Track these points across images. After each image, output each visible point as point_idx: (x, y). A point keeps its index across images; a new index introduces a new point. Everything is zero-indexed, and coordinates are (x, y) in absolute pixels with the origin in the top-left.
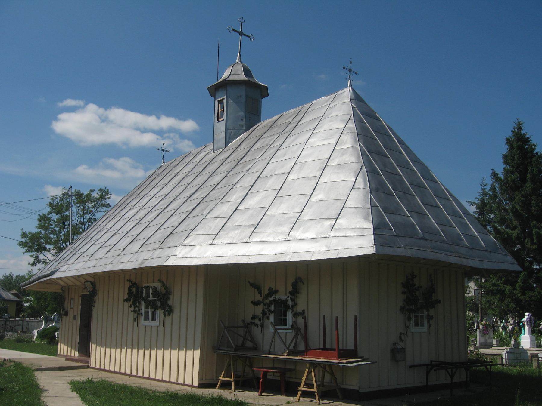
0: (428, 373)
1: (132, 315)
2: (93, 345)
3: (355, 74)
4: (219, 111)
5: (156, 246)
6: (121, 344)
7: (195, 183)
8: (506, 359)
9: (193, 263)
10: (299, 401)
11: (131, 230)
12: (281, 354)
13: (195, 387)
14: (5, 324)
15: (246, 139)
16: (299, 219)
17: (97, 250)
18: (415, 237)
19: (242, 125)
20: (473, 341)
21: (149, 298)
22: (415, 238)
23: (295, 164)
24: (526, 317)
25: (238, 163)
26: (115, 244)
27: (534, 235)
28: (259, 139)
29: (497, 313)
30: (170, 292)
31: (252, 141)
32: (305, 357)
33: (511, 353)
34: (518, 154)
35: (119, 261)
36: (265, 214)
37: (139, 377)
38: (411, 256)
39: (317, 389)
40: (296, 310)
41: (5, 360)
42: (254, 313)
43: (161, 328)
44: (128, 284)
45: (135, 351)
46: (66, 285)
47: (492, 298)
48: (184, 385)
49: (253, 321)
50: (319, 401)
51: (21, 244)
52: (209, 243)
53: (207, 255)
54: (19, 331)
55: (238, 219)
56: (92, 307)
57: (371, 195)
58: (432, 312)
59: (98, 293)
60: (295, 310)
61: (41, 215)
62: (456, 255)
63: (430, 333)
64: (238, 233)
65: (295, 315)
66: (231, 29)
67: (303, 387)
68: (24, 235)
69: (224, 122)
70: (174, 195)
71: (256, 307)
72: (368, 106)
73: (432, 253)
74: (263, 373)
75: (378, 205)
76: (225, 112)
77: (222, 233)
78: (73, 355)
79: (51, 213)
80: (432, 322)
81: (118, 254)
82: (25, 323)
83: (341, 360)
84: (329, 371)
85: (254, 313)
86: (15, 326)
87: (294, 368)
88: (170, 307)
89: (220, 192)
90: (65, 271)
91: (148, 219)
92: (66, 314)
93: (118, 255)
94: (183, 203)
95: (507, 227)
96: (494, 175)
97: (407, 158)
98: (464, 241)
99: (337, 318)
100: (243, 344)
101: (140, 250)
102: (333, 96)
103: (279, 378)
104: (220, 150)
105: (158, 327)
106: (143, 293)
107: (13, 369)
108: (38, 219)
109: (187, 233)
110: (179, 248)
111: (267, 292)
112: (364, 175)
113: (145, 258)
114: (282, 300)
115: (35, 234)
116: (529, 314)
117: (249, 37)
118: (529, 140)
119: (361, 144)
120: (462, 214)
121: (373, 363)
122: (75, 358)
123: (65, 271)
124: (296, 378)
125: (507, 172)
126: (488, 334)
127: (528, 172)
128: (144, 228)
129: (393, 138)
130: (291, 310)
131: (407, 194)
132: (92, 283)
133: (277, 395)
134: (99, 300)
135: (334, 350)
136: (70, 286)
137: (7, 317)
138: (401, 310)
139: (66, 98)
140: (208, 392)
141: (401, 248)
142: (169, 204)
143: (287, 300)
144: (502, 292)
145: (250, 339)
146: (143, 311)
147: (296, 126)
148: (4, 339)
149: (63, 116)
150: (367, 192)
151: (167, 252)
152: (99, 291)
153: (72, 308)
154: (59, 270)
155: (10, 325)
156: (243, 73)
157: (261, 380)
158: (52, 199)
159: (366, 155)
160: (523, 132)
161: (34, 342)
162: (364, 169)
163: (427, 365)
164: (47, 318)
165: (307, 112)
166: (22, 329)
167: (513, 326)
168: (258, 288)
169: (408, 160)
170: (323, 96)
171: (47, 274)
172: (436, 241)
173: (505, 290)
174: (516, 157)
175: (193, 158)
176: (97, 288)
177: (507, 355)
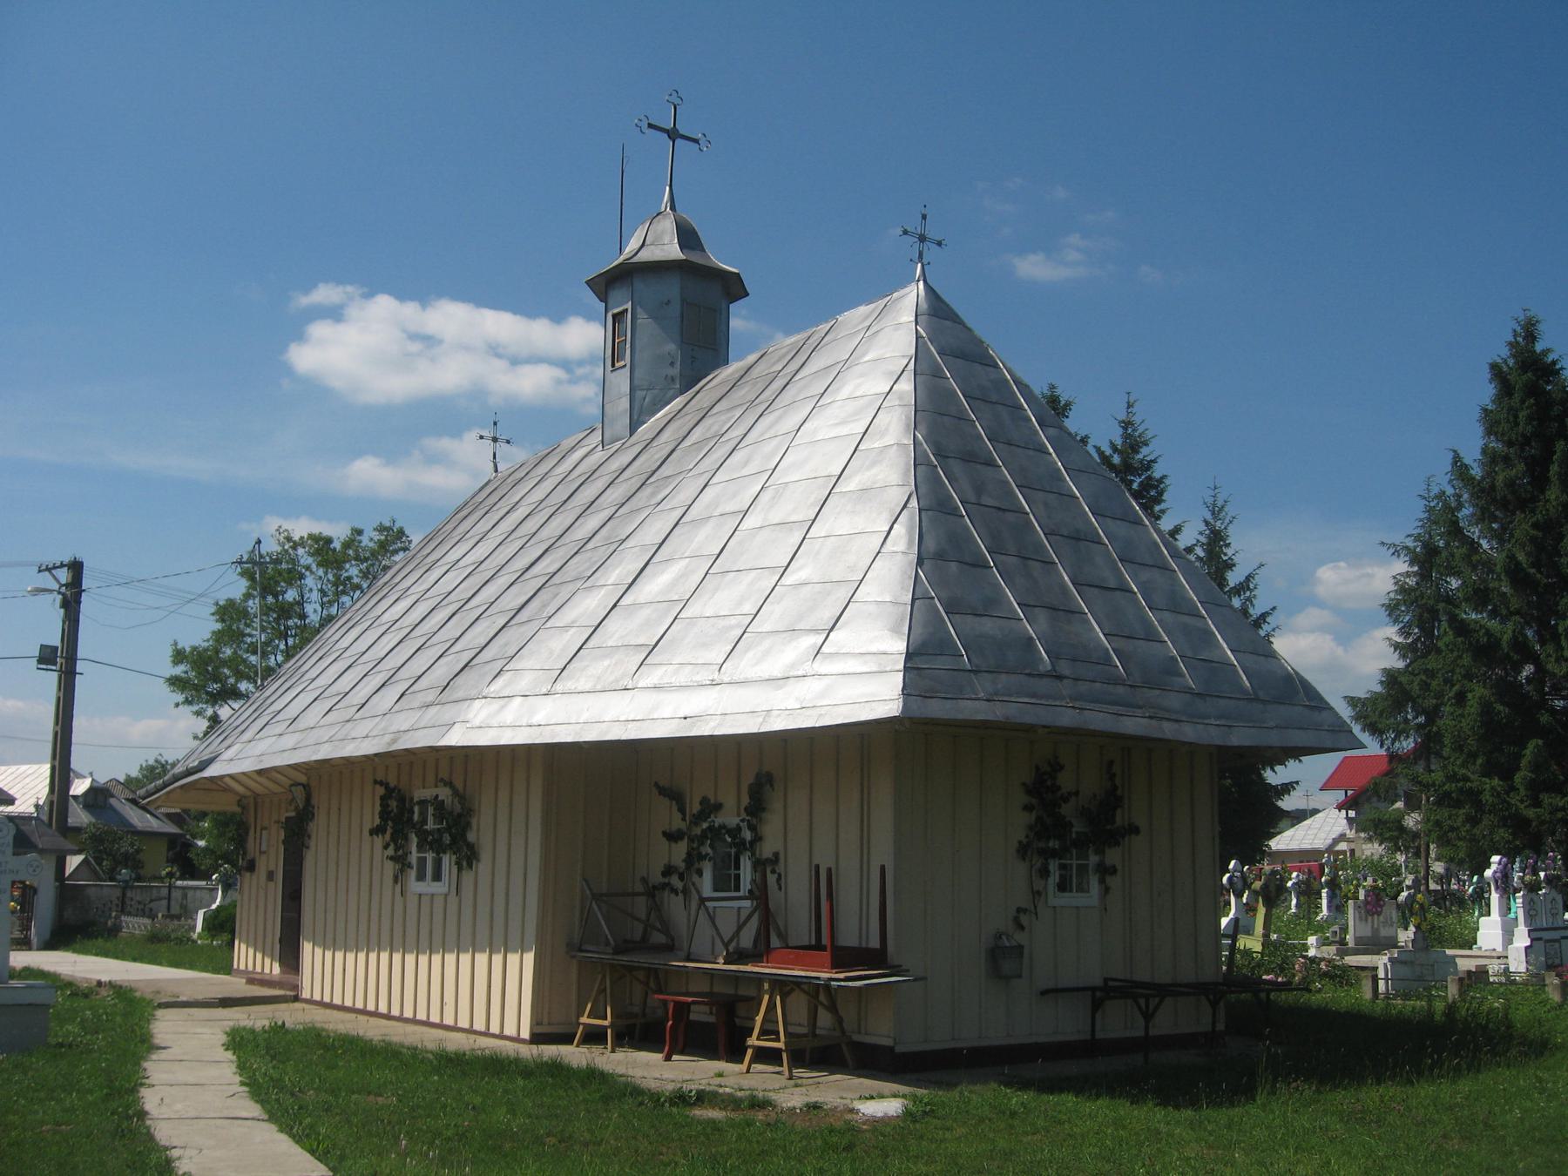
0: (1096, 1006)
1: (390, 867)
4: (617, 341)
5: (431, 696)
6: (366, 941)
7: (544, 533)
8: (1386, 979)
9: (503, 742)
10: (748, 1071)
11: (387, 655)
12: (713, 960)
13: (523, 1041)
14: (124, 895)
15: (678, 416)
16: (748, 630)
17: (308, 706)
18: (1027, 671)
19: (673, 379)
20: (1336, 932)
21: (427, 825)
22: (1026, 674)
23: (762, 488)
24: (1494, 867)
25: (646, 481)
26: (347, 691)
27: (1563, 637)
28: (703, 417)
29: (1462, 855)
30: (471, 810)
31: (690, 421)
32: (762, 967)
33: (1404, 963)
34: (1527, 408)
35: (346, 735)
36: (676, 618)
37: (407, 1021)
38: (1001, 719)
39: (786, 1043)
40: (761, 854)
41: (99, 983)
42: (670, 861)
43: (453, 898)
44: (381, 791)
45: (397, 957)
46: (249, 793)
47: (1446, 814)
48: (501, 1037)
49: (666, 880)
50: (790, 1071)
51: (175, 682)
52: (544, 690)
53: (535, 721)
54: (160, 915)
55: (615, 630)
56: (304, 849)
58: (1113, 856)
59: (316, 815)
60: (757, 853)
62: (1147, 715)
63: (1106, 909)
64: (609, 666)
65: (759, 865)
66: (647, 125)
67: (758, 1039)
68: (179, 656)
69: (627, 370)
70: (494, 564)
71: (673, 845)
73: (1070, 711)
74: (674, 1006)
75: (934, 595)
76: (628, 345)
77: (574, 665)
78: (267, 970)
80: (1114, 882)
81: (347, 718)
82: (176, 894)
83: (836, 973)
84: (825, 1003)
85: (670, 861)
86: (151, 901)
87: (755, 995)
88: (471, 847)
89: (591, 558)
90: (231, 760)
91: (429, 626)
92: (251, 867)
93: (348, 721)
94: (508, 588)
95: (1494, 614)
96: (1460, 469)
97: (1057, 464)
98: (1184, 676)
99: (883, 868)
100: (644, 938)
101: (397, 708)
102: (882, 303)
103: (712, 1019)
104: (618, 444)
105: (446, 895)
106: (413, 812)
107: (111, 1003)
109: (498, 665)
110: (477, 704)
111: (696, 808)
112: (911, 519)
113: (402, 729)
114: (729, 827)
115: (206, 650)
116: (1501, 859)
117: (696, 141)
118: (1557, 367)
119: (920, 437)
120: (1199, 605)
121: (915, 980)
122: (273, 979)
123: (231, 760)
125: (1492, 459)
126: (1379, 914)
127: (1555, 457)
128: (415, 649)
129: (1026, 410)
130: (749, 853)
132: (304, 786)
133: (711, 1059)
134: (318, 828)
136: (258, 795)
137: (128, 878)
138: (1018, 851)
141: (977, 702)
142: (480, 589)
143: (739, 829)
144: (1474, 796)
145: (658, 925)
146: (414, 857)
147: (788, 384)
148: (120, 934)
150: (911, 563)
151: (447, 713)
152: (318, 808)
153: (264, 852)
154: (218, 759)
155: (138, 898)
156: (676, 240)
157: (670, 1023)
159: (930, 464)
160: (1539, 347)
161: (194, 942)
162: (914, 503)
163: (1093, 989)
164: (227, 880)
165: (819, 347)
166: (169, 908)
167: (1413, 891)
168: (676, 797)
169: (1060, 469)
170: (861, 305)
171: (192, 768)
172: (1089, 681)
173: (1481, 792)
174: (1522, 414)
175: (559, 461)
176: (314, 801)
177: (1389, 967)
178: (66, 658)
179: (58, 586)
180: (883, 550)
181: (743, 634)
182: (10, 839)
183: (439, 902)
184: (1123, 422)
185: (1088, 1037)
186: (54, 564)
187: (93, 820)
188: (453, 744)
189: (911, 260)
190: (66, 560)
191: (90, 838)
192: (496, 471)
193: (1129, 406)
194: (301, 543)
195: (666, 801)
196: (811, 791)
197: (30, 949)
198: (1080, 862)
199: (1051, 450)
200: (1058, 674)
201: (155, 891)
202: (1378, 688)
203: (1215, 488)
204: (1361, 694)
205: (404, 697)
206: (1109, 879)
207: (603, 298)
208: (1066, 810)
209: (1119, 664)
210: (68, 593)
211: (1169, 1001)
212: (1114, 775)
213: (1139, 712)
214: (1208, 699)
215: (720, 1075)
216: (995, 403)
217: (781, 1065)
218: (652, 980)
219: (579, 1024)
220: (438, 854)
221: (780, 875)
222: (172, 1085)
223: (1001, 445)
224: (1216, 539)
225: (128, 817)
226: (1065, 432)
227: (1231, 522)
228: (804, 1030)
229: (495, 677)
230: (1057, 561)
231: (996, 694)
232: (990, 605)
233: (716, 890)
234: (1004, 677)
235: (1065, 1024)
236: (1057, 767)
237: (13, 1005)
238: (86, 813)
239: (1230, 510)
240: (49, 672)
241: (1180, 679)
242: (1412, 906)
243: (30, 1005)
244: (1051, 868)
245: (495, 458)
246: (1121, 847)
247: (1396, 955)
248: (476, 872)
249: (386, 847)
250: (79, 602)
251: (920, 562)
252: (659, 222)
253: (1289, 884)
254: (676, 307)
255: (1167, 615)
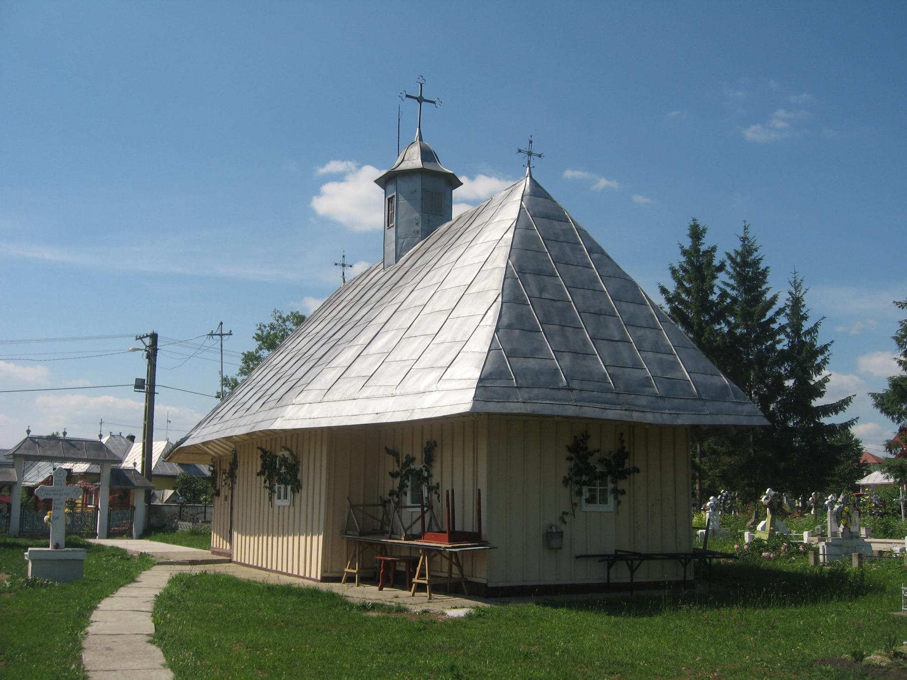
2: (234, 532)
3: (538, 157)
4: (390, 213)
5: (272, 404)
8: (824, 555)
10: (413, 595)
18: (551, 387)
19: (418, 232)
32: (421, 542)
36: (383, 362)
43: (292, 509)
45: (275, 539)
46: (216, 455)
50: (430, 595)
52: (319, 400)
53: (314, 415)
54: (200, 521)
57: (496, 335)
58: (622, 484)
61: (246, 353)
63: (618, 513)
65: (430, 489)
67: (418, 579)
71: (395, 480)
72: (555, 202)
74: (384, 562)
79: (261, 349)
81: (241, 416)
86: (198, 514)
97: (596, 273)
99: (448, 491)
105: (289, 506)
108: (243, 359)
117: (434, 102)
120: (673, 348)
124: (441, 572)
131: (567, 328)
135: (445, 532)
136: (221, 456)
137: (183, 502)
138: (563, 482)
139: (328, 161)
140: (324, 586)
143: (421, 471)
149: (328, 188)
157: (382, 571)
158: (260, 329)
162: (500, 299)
168: (395, 454)
169: (597, 276)
176: (238, 459)
177: (825, 548)
178: (150, 385)
179: (145, 347)
180: (480, 325)
181: (410, 369)
182: (65, 478)
183: (286, 509)
184: (742, 238)
185: (606, 581)
186: (143, 335)
187: (183, 471)
188: (275, 428)
189: (524, 166)
190: (149, 334)
191: (181, 481)
192: (344, 282)
193: (746, 228)
194: (288, 319)
195: (391, 457)
196: (453, 452)
197: (132, 539)
198: (606, 488)
199: (593, 266)
200: (570, 388)
201: (199, 508)
202: (888, 388)
203: (795, 273)
204: (881, 392)
205: (264, 405)
206: (620, 497)
207: (384, 187)
208: (592, 461)
209: (611, 382)
210: (150, 350)
211: (645, 562)
212: (623, 441)
213: (619, 407)
214: (667, 399)
215: (397, 597)
216: (563, 242)
217: (426, 592)
218: (453, 557)
219: (344, 572)
220: (286, 485)
221: (439, 495)
222: (122, 597)
223: (562, 265)
224: (797, 303)
225: (202, 470)
226: (606, 255)
227: (805, 292)
228: (446, 575)
229: (299, 394)
230: (584, 327)
231: (529, 399)
232: (536, 352)
233: (412, 503)
234: (536, 390)
235: (594, 574)
236: (586, 437)
237: (64, 560)
238: (180, 468)
239: (804, 286)
240: (141, 393)
241: (651, 389)
242: (842, 514)
243: (74, 560)
244: (584, 491)
245: (343, 275)
246: (628, 479)
247: (830, 541)
248: (301, 494)
249: (265, 482)
250: (155, 355)
251: (497, 330)
252: (412, 148)
253: (826, 502)
254: (419, 195)
255: (650, 355)
